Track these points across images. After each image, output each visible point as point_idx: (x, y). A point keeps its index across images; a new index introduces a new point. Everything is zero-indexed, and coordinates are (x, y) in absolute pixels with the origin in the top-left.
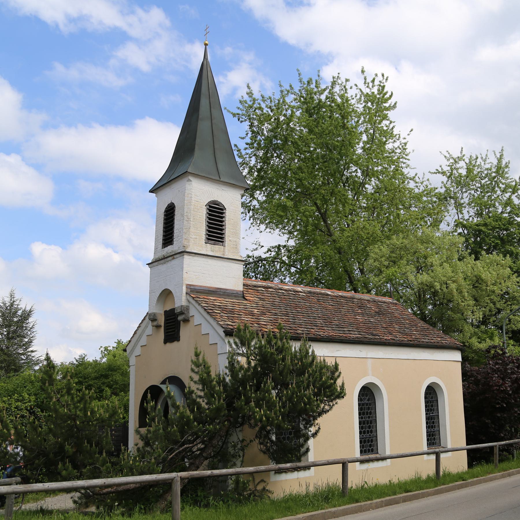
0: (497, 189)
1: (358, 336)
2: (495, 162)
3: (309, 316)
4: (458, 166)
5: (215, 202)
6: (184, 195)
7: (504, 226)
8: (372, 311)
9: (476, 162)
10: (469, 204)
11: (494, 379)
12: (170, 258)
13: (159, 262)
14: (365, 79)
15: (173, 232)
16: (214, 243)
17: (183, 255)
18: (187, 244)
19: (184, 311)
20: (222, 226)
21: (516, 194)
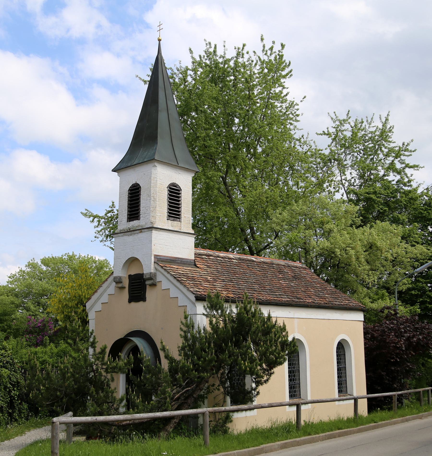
0: (379, 152)
1: (288, 299)
2: (380, 126)
3: (247, 282)
4: (343, 128)
5: (174, 185)
6: (150, 178)
7: (392, 194)
8: (289, 275)
9: (361, 126)
10: (352, 166)
11: (391, 337)
12: (138, 231)
13: (125, 233)
14: (264, 47)
15: (139, 209)
16: (174, 219)
17: (152, 230)
18: (154, 220)
19: (152, 277)
20: (179, 204)
21: (399, 159)
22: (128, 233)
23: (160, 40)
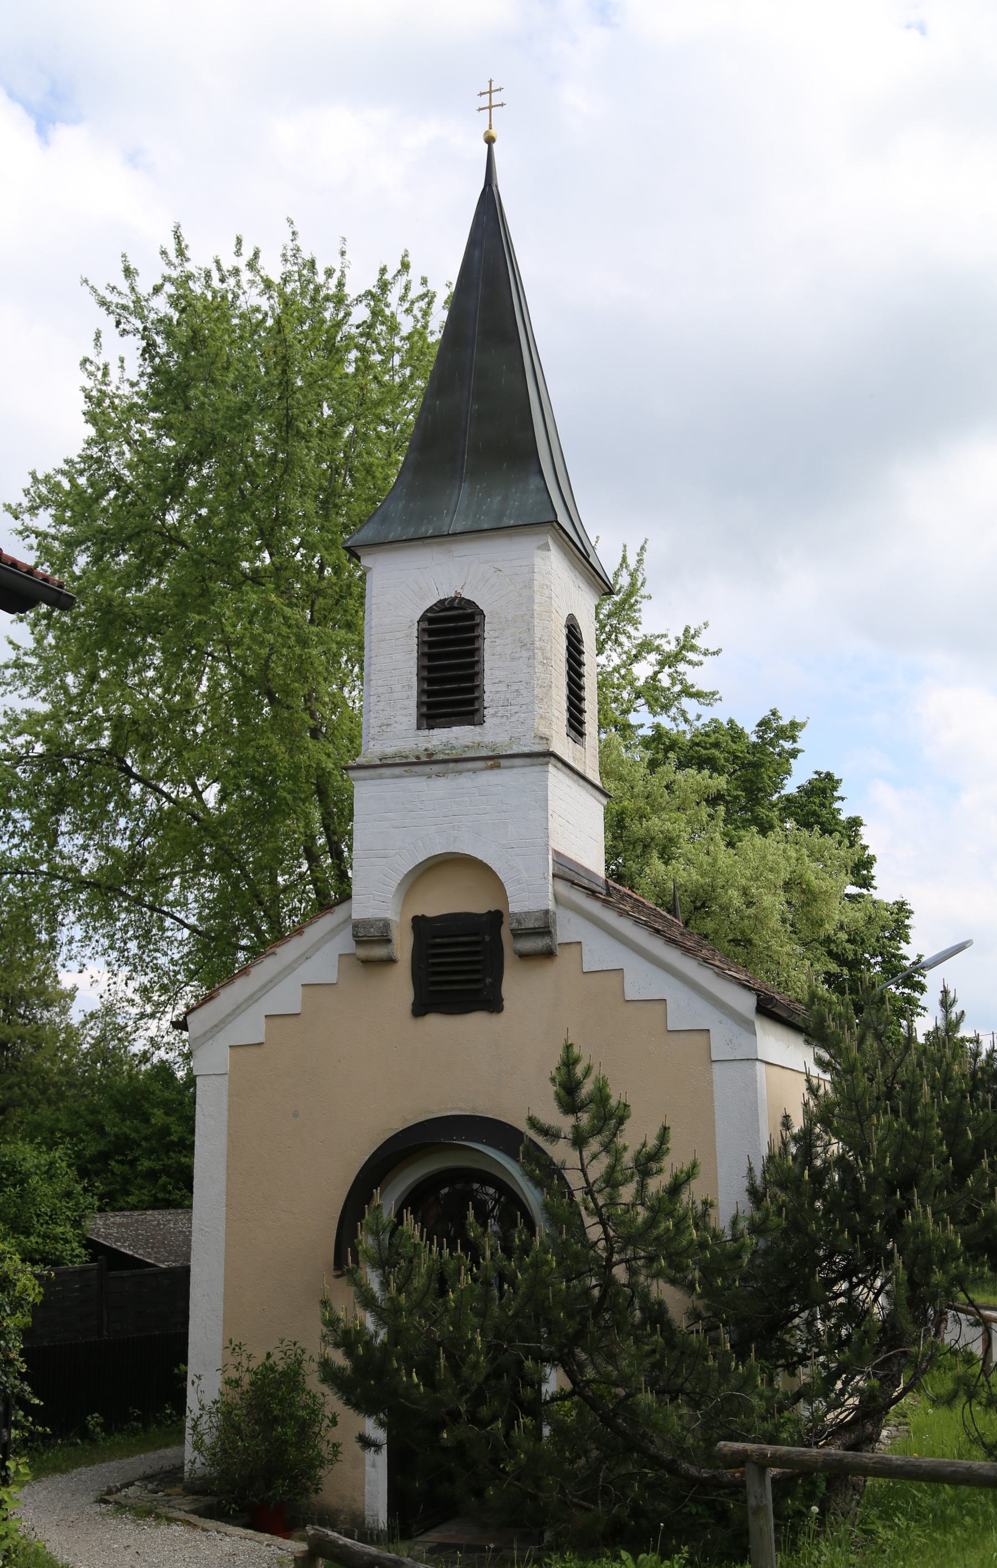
17: (547, 763)
22: (427, 769)
23: (490, 140)
